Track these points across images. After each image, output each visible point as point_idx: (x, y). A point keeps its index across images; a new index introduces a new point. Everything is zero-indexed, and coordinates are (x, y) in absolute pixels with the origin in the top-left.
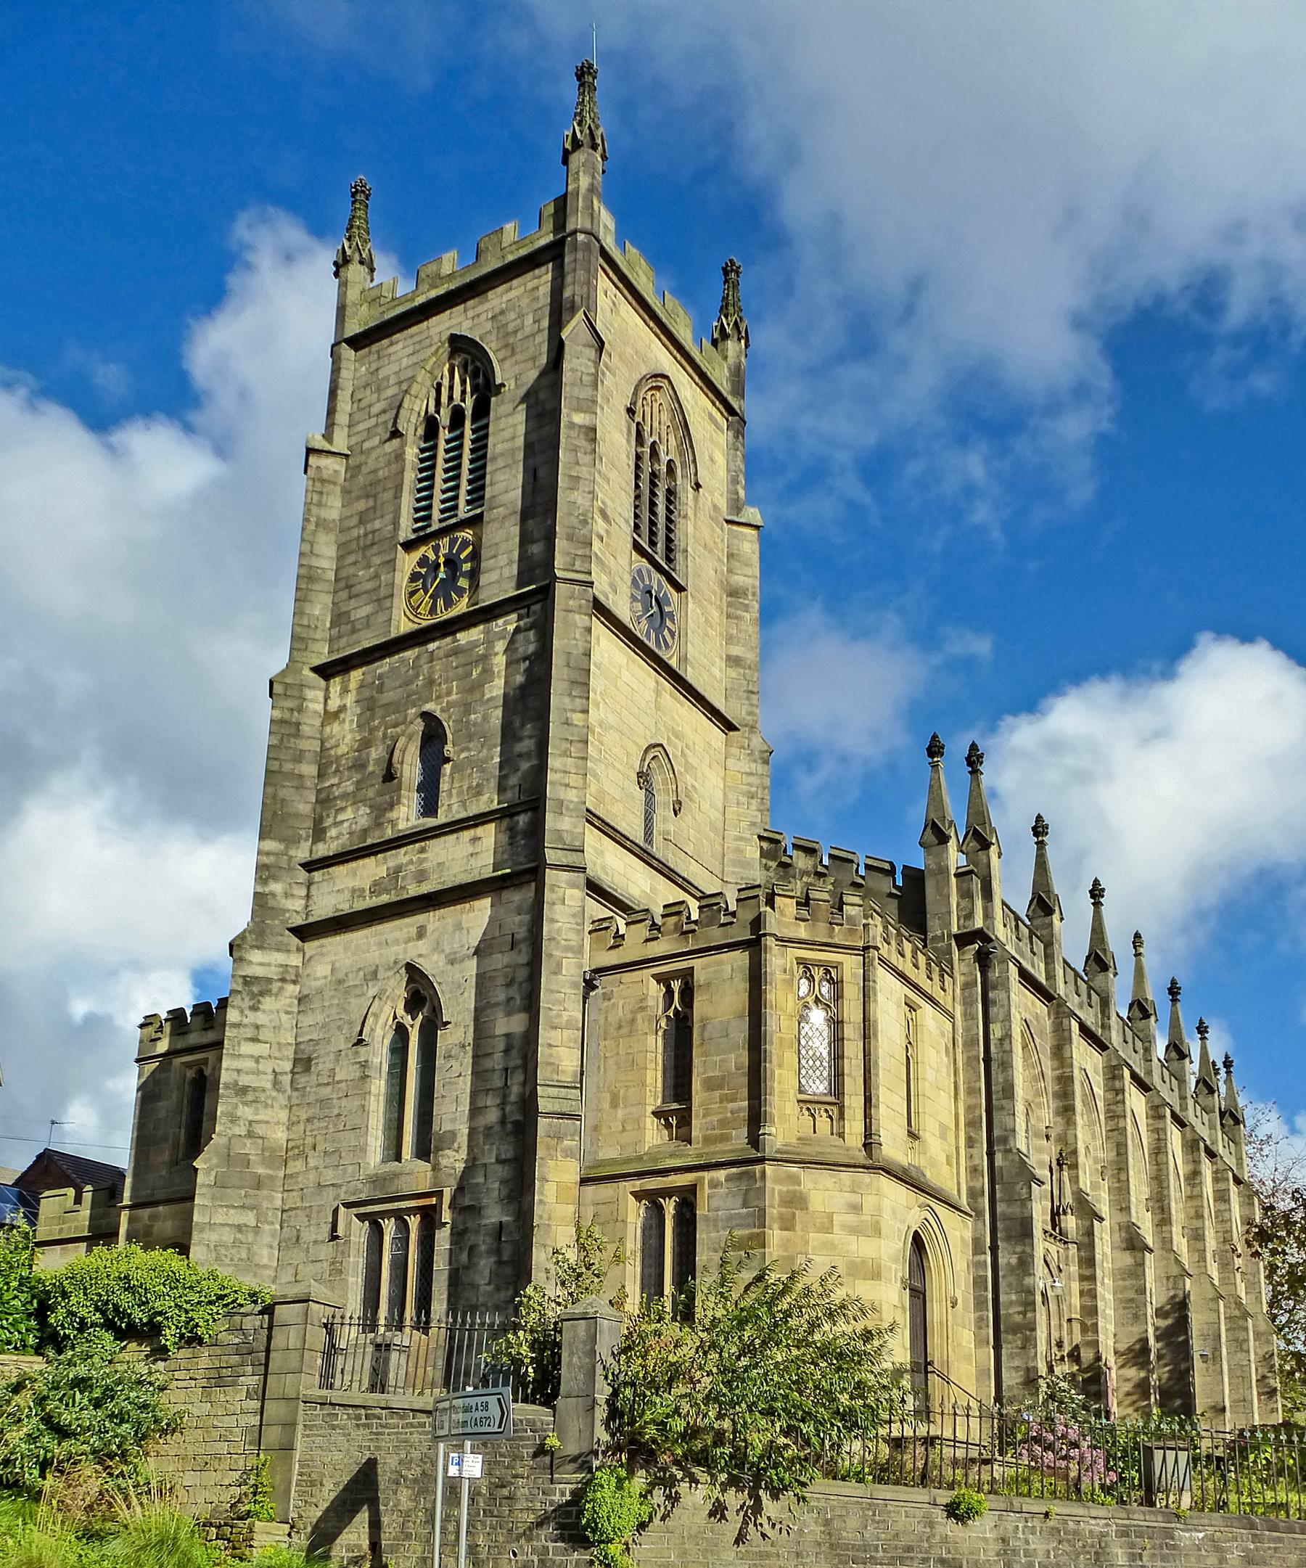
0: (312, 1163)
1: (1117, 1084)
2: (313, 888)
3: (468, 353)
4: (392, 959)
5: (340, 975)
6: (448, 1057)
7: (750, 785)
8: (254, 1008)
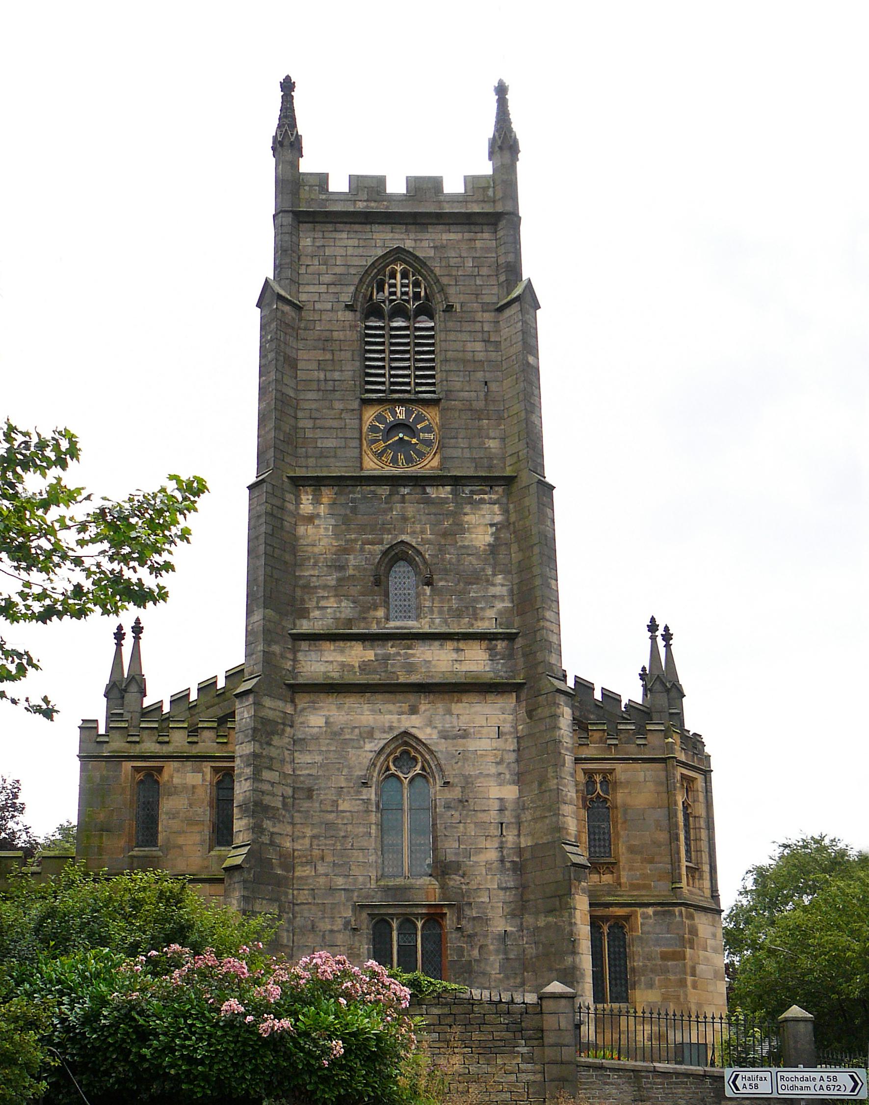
0: (321, 869)
3: (411, 265)
4: (387, 725)
8: (269, 744)
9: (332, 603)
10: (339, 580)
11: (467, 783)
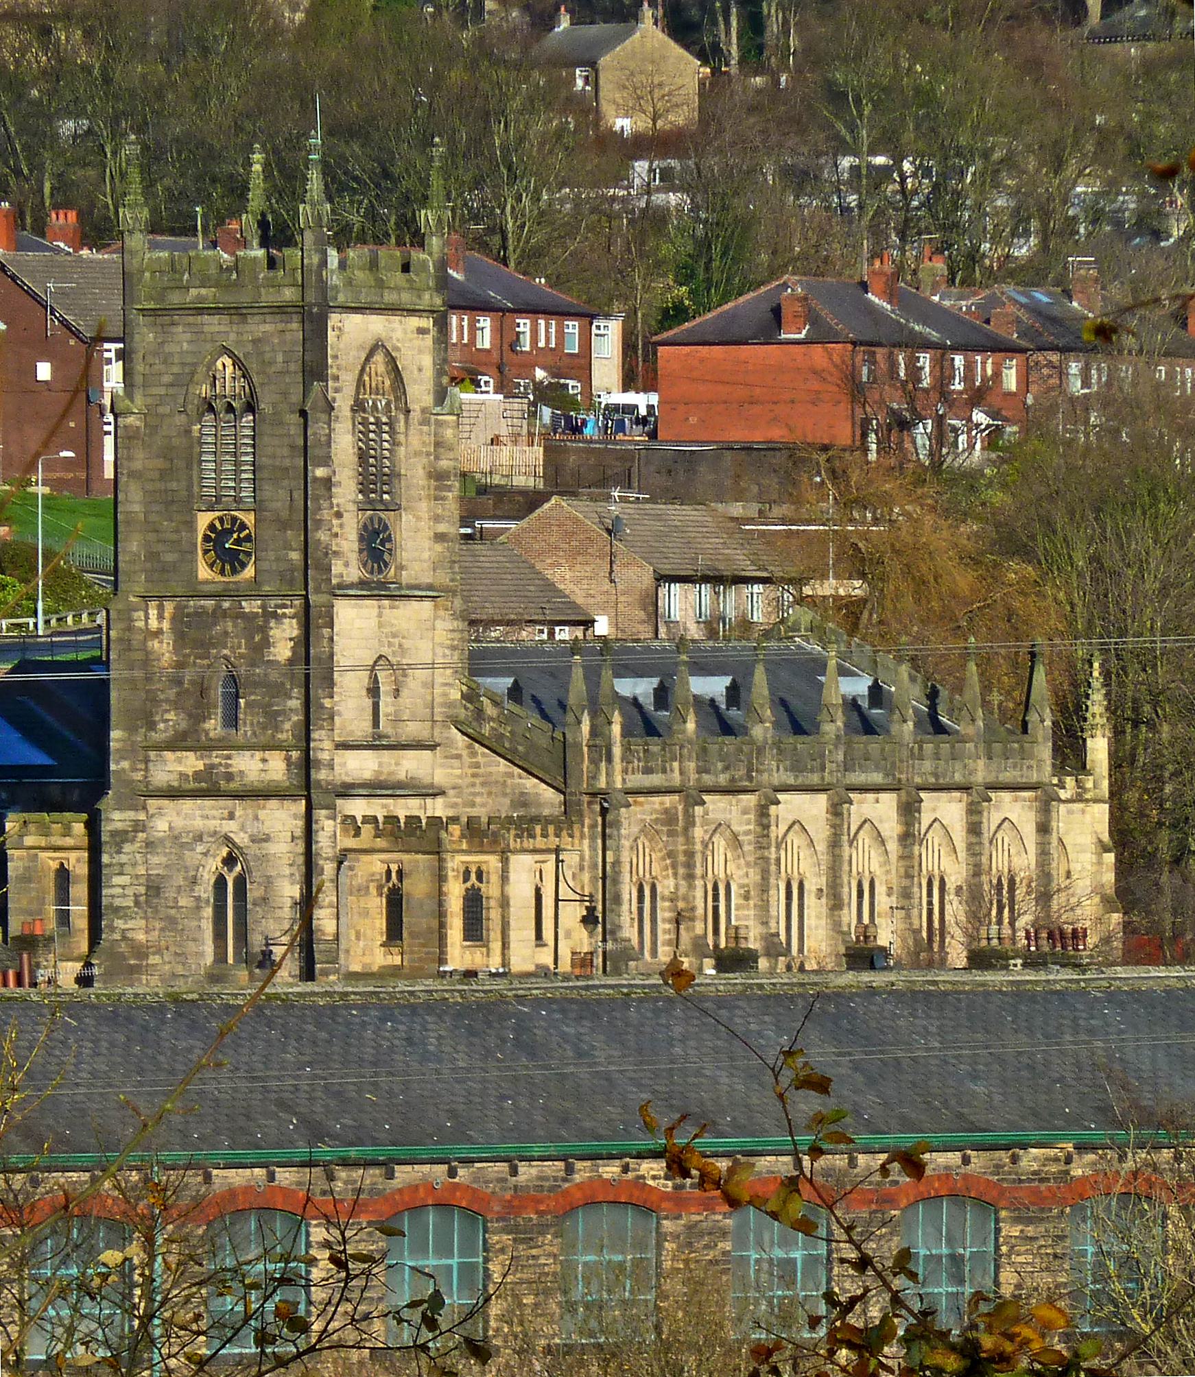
1: (765, 821)
2: (151, 764)
5: (176, 833)
6: (254, 904)
7: (453, 639)
8: (119, 852)
9: (171, 716)
10: (178, 694)
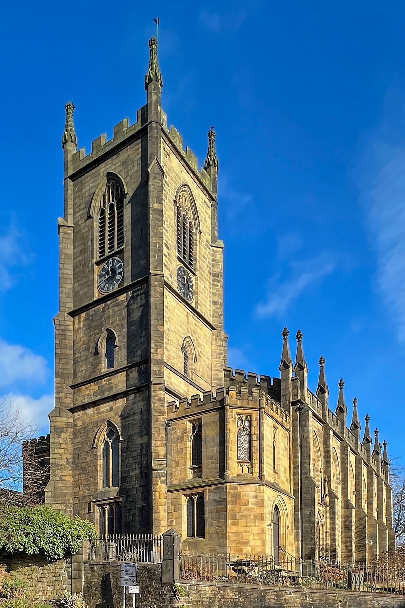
8: (59, 437)
11: (130, 439)
